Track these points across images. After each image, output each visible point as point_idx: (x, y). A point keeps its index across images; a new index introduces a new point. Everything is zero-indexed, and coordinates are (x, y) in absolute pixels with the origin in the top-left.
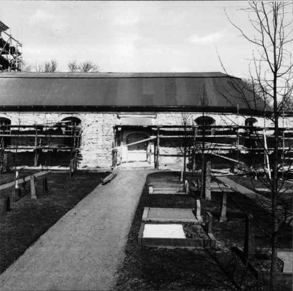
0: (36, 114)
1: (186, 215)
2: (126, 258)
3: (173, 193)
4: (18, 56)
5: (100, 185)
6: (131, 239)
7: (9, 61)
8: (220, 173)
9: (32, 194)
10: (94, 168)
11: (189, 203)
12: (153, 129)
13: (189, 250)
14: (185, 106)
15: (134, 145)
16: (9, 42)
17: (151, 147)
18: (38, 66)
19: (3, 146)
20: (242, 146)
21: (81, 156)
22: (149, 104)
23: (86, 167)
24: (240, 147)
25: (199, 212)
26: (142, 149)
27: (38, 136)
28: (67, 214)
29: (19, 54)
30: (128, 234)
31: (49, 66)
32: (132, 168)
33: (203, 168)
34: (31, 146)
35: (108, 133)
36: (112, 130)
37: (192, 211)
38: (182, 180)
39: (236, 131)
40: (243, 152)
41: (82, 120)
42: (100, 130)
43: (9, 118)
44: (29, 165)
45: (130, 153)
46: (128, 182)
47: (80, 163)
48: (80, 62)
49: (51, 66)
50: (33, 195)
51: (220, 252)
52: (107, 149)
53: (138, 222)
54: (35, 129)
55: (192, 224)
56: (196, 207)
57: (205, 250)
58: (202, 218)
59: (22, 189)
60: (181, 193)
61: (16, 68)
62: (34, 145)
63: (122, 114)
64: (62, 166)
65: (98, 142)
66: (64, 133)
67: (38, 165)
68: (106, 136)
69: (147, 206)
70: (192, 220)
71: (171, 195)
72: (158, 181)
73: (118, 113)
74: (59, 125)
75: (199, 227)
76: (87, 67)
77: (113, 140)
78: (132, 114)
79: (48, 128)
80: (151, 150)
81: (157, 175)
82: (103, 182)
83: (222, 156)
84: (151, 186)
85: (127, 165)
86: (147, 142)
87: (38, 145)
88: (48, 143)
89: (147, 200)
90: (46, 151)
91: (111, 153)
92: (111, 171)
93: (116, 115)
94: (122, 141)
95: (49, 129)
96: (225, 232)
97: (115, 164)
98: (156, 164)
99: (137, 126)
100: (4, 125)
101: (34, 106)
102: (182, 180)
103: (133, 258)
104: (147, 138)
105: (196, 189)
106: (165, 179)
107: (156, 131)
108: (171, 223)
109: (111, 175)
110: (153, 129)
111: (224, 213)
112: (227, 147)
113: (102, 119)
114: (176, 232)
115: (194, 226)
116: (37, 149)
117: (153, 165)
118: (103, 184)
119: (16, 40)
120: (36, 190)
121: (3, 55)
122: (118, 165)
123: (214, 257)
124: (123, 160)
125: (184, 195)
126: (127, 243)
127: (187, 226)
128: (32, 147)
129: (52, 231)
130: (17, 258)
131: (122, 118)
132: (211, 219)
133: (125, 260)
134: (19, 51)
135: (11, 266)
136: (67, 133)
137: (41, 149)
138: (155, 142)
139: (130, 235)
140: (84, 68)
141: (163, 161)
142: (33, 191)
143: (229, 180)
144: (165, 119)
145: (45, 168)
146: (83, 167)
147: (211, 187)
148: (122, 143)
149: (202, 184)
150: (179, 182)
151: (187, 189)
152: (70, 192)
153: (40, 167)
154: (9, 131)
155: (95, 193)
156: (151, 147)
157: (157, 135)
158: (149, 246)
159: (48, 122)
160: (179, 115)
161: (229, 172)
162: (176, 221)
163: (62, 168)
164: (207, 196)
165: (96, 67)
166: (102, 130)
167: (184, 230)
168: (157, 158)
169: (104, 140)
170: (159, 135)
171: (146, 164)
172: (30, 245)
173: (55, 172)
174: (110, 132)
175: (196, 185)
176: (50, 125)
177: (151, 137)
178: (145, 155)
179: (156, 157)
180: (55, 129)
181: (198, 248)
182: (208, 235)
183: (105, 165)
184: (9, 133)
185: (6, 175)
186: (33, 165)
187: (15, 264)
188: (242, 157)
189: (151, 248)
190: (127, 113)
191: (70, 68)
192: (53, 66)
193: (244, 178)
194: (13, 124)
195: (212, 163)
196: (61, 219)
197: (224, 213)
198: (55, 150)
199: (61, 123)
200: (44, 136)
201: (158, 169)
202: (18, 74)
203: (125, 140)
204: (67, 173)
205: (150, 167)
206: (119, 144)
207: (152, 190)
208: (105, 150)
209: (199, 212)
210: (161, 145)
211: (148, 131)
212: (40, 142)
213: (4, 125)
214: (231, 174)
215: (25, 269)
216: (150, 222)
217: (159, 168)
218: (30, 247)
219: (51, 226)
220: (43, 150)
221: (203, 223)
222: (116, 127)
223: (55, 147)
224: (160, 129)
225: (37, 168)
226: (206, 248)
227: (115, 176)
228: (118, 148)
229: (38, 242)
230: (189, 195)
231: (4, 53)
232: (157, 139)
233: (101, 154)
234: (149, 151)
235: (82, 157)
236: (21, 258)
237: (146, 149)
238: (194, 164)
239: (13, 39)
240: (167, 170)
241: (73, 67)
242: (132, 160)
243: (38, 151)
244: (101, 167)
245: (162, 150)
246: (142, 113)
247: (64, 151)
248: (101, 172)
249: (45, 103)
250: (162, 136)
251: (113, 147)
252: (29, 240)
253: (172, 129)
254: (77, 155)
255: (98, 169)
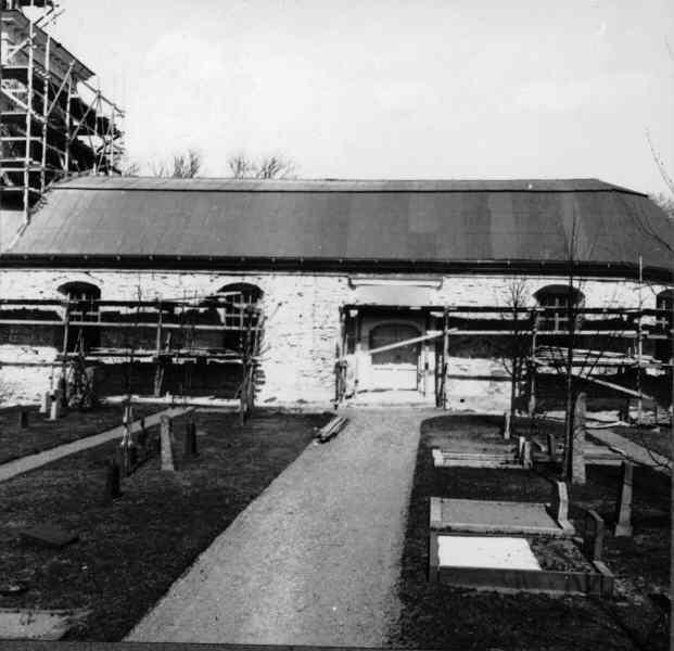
0: (159, 275)
1: (534, 518)
2: (403, 610)
3: (492, 466)
4: (115, 139)
5: (315, 443)
6: (409, 568)
7: (95, 150)
8: (594, 420)
9: (164, 460)
10: (293, 403)
11: (534, 489)
12: (432, 313)
13: (552, 597)
14: (511, 260)
15: (390, 351)
16: (94, 107)
17: (428, 356)
18: (157, 164)
19: (82, 350)
20: (650, 357)
21: (261, 374)
22: (427, 256)
23: (273, 399)
24: (643, 359)
25: (563, 511)
26: (406, 361)
27: (164, 325)
28: (250, 508)
29: (118, 134)
30: (400, 557)
31: (182, 162)
32: (383, 405)
33: (569, 408)
34: (147, 349)
35: (326, 322)
36: (337, 315)
37: (544, 509)
38: (507, 435)
39: (636, 321)
40: (652, 372)
41: (266, 292)
42: (307, 314)
43: (97, 283)
44: (143, 394)
45: (376, 369)
46: (380, 439)
47: (259, 391)
48: (256, 157)
49: (187, 162)
50: (168, 462)
51: (625, 604)
52: (323, 359)
53: (419, 533)
54: (158, 311)
55: (549, 538)
56: (556, 500)
57: (587, 598)
58: (575, 525)
59: (139, 447)
60: (510, 466)
61: (110, 167)
62: (154, 347)
63: (361, 279)
64: (217, 397)
65: (302, 342)
66: (223, 320)
67: (162, 394)
68: (321, 328)
69: (436, 496)
70: (546, 526)
71: (487, 470)
72: (449, 437)
73: (351, 276)
74: (211, 302)
75: (569, 546)
76: (270, 169)
77: (338, 339)
78: (401, 279)
79: (186, 309)
80: (427, 366)
81: (444, 424)
82: (319, 437)
83: (597, 381)
84: (437, 448)
85: (373, 400)
86: (419, 346)
87: (163, 347)
88: (187, 343)
89: (431, 482)
90: (182, 361)
91: (332, 369)
92: (333, 411)
93: (345, 281)
94: (359, 340)
95: (189, 311)
96: (626, 557)
97: (342, 396)
98: (440, 398)
99: (396, 307)
100: (84, 298)
101: (154, 256)
102: (507, 435)
103: (423, 612)
104: (419, 334)
105: (547, 459)
106: (466, 433)
107: (440, 318)
108: (498, 534)
109: (337, 420)
110: (432, 313)
111: (625, 514)
112: (613, 358)
113: (311, 290)
114: (516, 555)
115: (555, 543)
116: (161, 358)
117: (431, 399)
118: (322, 442)
119: (112, 102)
120: (173, 451)
121: (80, 138)
122: (349, 397)
123: (614, 614)
124: (360, 388)
125: (518, 469)
126: (400, 578)
127: (537, 542)
128: (149, 352)
129: (223, 545)
130: (154, 601)
131: (361, 288)
132: (600, 527)
133: (402, 616)
134: (118, 128)
135: (145, 619)
136: (229, 321)
137: (171, 357)
138: (437, 345)
139: (407, 559)
140: (264, 169)
141: (454, 389)
142: (166, 453)
143: (618, 437)
144: (462, 290)
145: (179, 401)
146: (266, 401)
147: (583, 456)
148: (358, 346)
149: (568, 446)
150: (500, 441)
151: (527, 456)
152: (248, 457)
153: (168, 399)
154: (95, 314)
155: (308, 463)
156: (428, 356)
157: (443, 329)
158: (458, 586)
159: (188, 295)
160: (497, 281)
161: (617, 419)
162: (510, 531)
163: (217, 402)
164: (575, 474)
165: (292, 165)
166: (313, 315)
167: (533, 550)
168: (443, 383)
169: (318, 337)
170: (450, 328)
171: (416, 397)
172: (179, 576)
173: (203, 410)
174: (331, 319)
175: (544, 449)
176: (191, 302)
177: (428, 332)
178: (414, 375)
179: (440, 380)
180: (202, 310)
181: (574, 593)
182: (594, 566)
183: (320, 397)
184: (95, 319)
185: (91, 415)
186: (150, 393)
187: (151, 614)
188: (649, 384)
189: (460, 591)
190: (371, 275)
191: (232, 166)
192: (192, 164)
193: (655, 433)
194: (105, 297)
195: (589, 397)
196: (238, 518)
197: (625, 514)
198: (202, 359)
199: (218, 297)
200: (177, 326)
201: (446, 410)
202: (112, 181)
203: (367, 340)
204: (232, 415)
205: (425, 404)
206: (352, 350)
207: (441, 457)
208: (319, 361)
209: (563, 511)
210: (452, 353)
211: (426, 316)
212: (168, 342)
213: (84, 298)
214: (623, 424)
215: (177, 627)
216: (449, 531)
217: (448, 406)
218: (179, 580)
219: (218, 533)
220: (174, 360)
221: (575, 536)
222: (346, 309)
223: (203, 352)
224: (451, 314)
225: (160, 400)
226: (591, 593)
227: (345, 423)
228: (349, 358)
229: (194, 569)
230: (532, 470)
231: (83, 132)
232: (442, 337)
233: (308, 371)
234: (423, 368)
235: (264, 377)
236: (164, 602)
237: (415, 362)
238: (533, 398)
239: (104, 99)
240: (468, 410)
241: (240, 166)
242: (382, 386)
243: (163, 361)
244: (309, 400)
245: (454, 364)
246: (408, 276)
247: (222, 361)
248: (311, 412)
249: (151, 250)
250: (455, 331)
251: (338, 355)
252: (174, 564)
253: (479, 316)
254: (254, 372)
255: (303, 406)
